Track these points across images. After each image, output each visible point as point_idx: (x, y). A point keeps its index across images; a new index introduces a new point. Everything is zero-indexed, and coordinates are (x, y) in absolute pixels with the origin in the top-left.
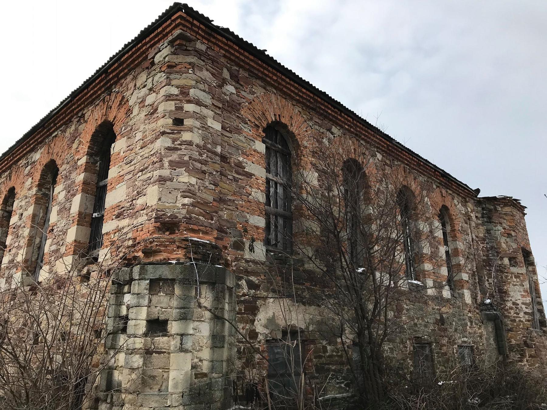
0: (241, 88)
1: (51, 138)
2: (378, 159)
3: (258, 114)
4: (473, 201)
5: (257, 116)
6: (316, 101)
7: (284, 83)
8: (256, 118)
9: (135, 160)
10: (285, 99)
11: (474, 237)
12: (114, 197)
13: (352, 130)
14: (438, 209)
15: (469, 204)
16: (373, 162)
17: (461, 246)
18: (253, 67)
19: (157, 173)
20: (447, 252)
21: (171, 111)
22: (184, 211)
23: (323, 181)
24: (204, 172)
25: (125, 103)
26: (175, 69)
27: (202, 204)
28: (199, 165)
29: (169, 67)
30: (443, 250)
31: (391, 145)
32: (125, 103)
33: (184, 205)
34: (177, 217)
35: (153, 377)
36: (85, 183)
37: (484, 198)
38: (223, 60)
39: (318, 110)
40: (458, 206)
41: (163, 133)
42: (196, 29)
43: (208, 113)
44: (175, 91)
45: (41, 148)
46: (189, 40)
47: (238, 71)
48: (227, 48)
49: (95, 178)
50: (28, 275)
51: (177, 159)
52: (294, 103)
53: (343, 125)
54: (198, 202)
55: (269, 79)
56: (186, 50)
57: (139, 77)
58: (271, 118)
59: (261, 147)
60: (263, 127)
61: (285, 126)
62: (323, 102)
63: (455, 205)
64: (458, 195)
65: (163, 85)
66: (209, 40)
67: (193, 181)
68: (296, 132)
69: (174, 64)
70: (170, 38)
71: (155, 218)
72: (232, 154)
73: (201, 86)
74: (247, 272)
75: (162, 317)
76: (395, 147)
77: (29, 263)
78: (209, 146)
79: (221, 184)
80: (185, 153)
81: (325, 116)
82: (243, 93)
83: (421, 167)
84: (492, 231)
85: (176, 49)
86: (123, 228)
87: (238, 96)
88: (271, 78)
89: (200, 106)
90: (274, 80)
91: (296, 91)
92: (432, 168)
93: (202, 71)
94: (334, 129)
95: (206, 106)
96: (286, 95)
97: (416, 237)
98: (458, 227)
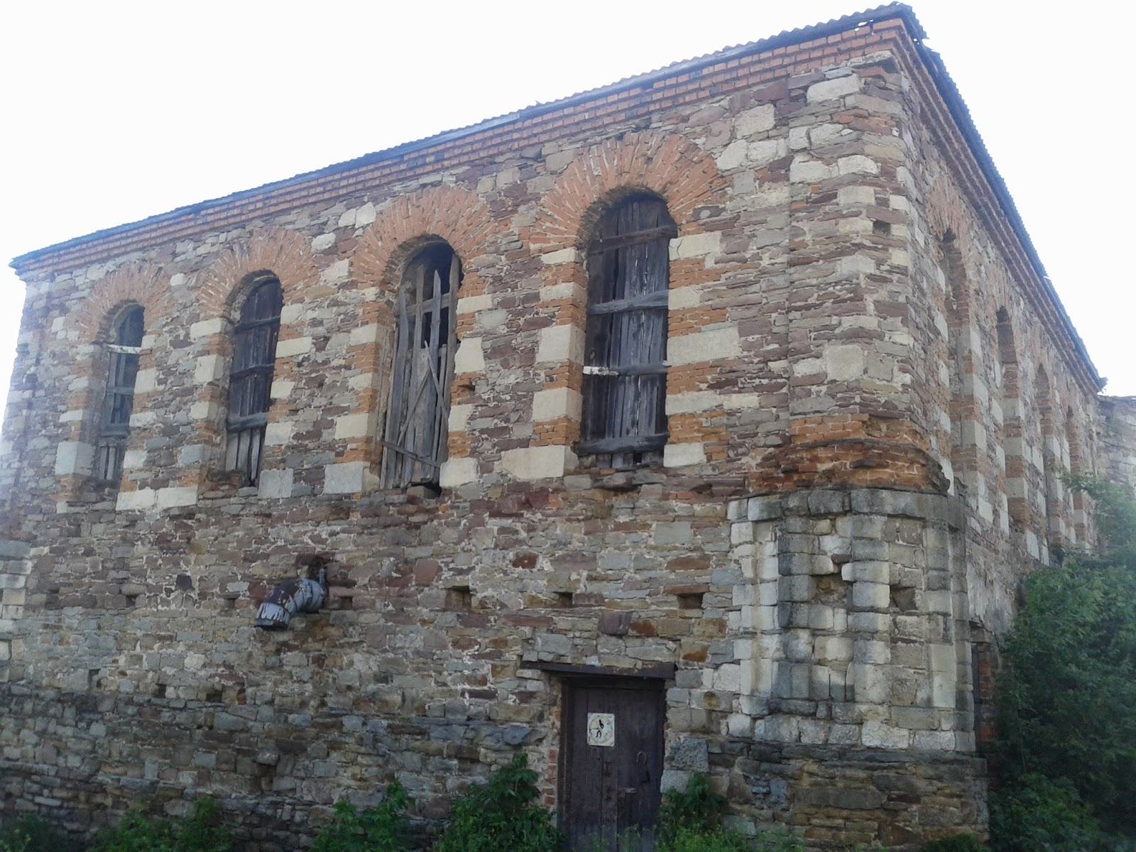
1: (414, 184)
21: (869, 206)
34: (896, 408)
51: (887, 299)
69: (866, 114)
70: (858, 60)
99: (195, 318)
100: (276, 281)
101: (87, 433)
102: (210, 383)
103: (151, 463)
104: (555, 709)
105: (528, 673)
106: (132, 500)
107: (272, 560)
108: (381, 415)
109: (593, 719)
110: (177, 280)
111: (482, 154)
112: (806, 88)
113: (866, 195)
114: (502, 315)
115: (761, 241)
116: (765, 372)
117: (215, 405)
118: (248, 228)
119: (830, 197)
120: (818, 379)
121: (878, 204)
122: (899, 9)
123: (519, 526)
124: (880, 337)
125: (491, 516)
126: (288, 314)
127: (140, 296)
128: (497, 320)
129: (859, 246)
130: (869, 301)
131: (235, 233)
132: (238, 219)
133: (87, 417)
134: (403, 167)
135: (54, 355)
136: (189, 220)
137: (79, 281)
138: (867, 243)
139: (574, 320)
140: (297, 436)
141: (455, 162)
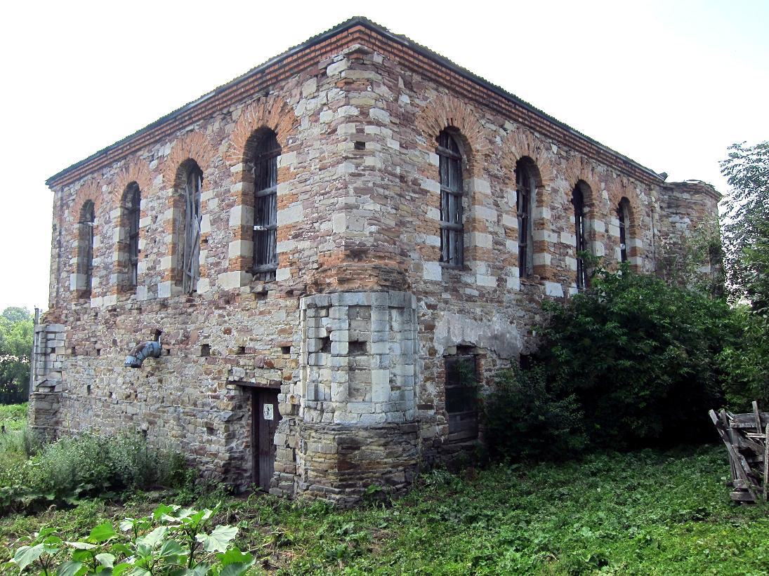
0: (415, 95)
1: (184, 131)
2: (553, 152)
3: (431, 122)
4: (658, 188)
5: (430, 125)
6: (489, 96)
7: (457, 82)
8: (429, 128)
9: (311, 180)
10: (458, 97)
11: (656, 232)
12: (285, 217)
13: (526, 122)
14: (617, 205)
15: (654, 193)
16: (546, 157)
17: (639, 243)
18: (426, 70)
19: (342, 201)
20: (623, 252)
21: (352, 134)
22: (372, 239)
23: (495, 187)
24: (386, 197)
25: (289, 112)
26: (353, 86)
27: (386, 230)
28: (381, 191)
29: (347, 83)
30: (618, 250)
31: (568, 134)
32: (289, 112)
33: (371, 233)
34: (365, 245)
35: (358, 390)
36: (244, 194)
38: (398, 69)
39: (491, 105)
40: (640, 197)
41: (346, 158)
42: (373, 41)
43: (387, 132)
44: (355, 112)
45: (170, 141)
46: (366, 53)
47: (412, 76)
48: (402, 54)
49: (252, 186)
50: (176, 284)
51: (362, 186)
52: (466, 101)
53: (517, 118)
54: (383, 229)
55: (442, 80)
56: (363, 64)
57: (305, 84)
59: (434, 159)
60: (436, 135)
61: (457, 130)
62: (497, 96)
63: (637, 196)
64: (642, 182)
65: (342, 104)
66: (384, 50)
67: (378, 207)
69: (351, 81)
70: (346, 51)
71: (345, 246)
72: (409, 172)
73: (380, 104)
74: (426, 293)
75: (361, 339)
76: (573, 136)
77: (176, 272)
78: (390, 169)
79: (401, 206)
80: (370, 180)
81: (498, 111)
82: (417, 101)
83: (601, 156)
84: (677, 224)
85: (352, 63)
86: (304, 250)
87: (412, 105)
88: (444, 79)
89: (380, 126)
90: (447, 81)
91: (469, 89)
92: (614, 155)
93: (380, 87)
94: (508, 125)
95: (385, 126)
96: (457, 94)
97: (576, 541)
98: (638, 222)
101: (81, 269)
102: (118, 242)
104: (249, 403)
105: (230, 387)
107: (143, 331)
108: (180, 256)
109: (266, 406)
111: (207, 113)
112: (326, 68)
115: (311, 156)
116: (312, 229)
117: (122, 253)
118: (128, 159)
119: (334, 131)
121: (357, 132)
122: (357, 20)
123: (225, 313)
124: (357, 207)
125: (216, 309)
127: (92, 198)
128: (213, 205)
131: (123, 162)
132: (122, 155)
133: (80, 261)
134: (177, 123)
135: (66, 230)
136: (104, 157)
138: (351, 156)
139: (244, 202)
141: (197, 118)
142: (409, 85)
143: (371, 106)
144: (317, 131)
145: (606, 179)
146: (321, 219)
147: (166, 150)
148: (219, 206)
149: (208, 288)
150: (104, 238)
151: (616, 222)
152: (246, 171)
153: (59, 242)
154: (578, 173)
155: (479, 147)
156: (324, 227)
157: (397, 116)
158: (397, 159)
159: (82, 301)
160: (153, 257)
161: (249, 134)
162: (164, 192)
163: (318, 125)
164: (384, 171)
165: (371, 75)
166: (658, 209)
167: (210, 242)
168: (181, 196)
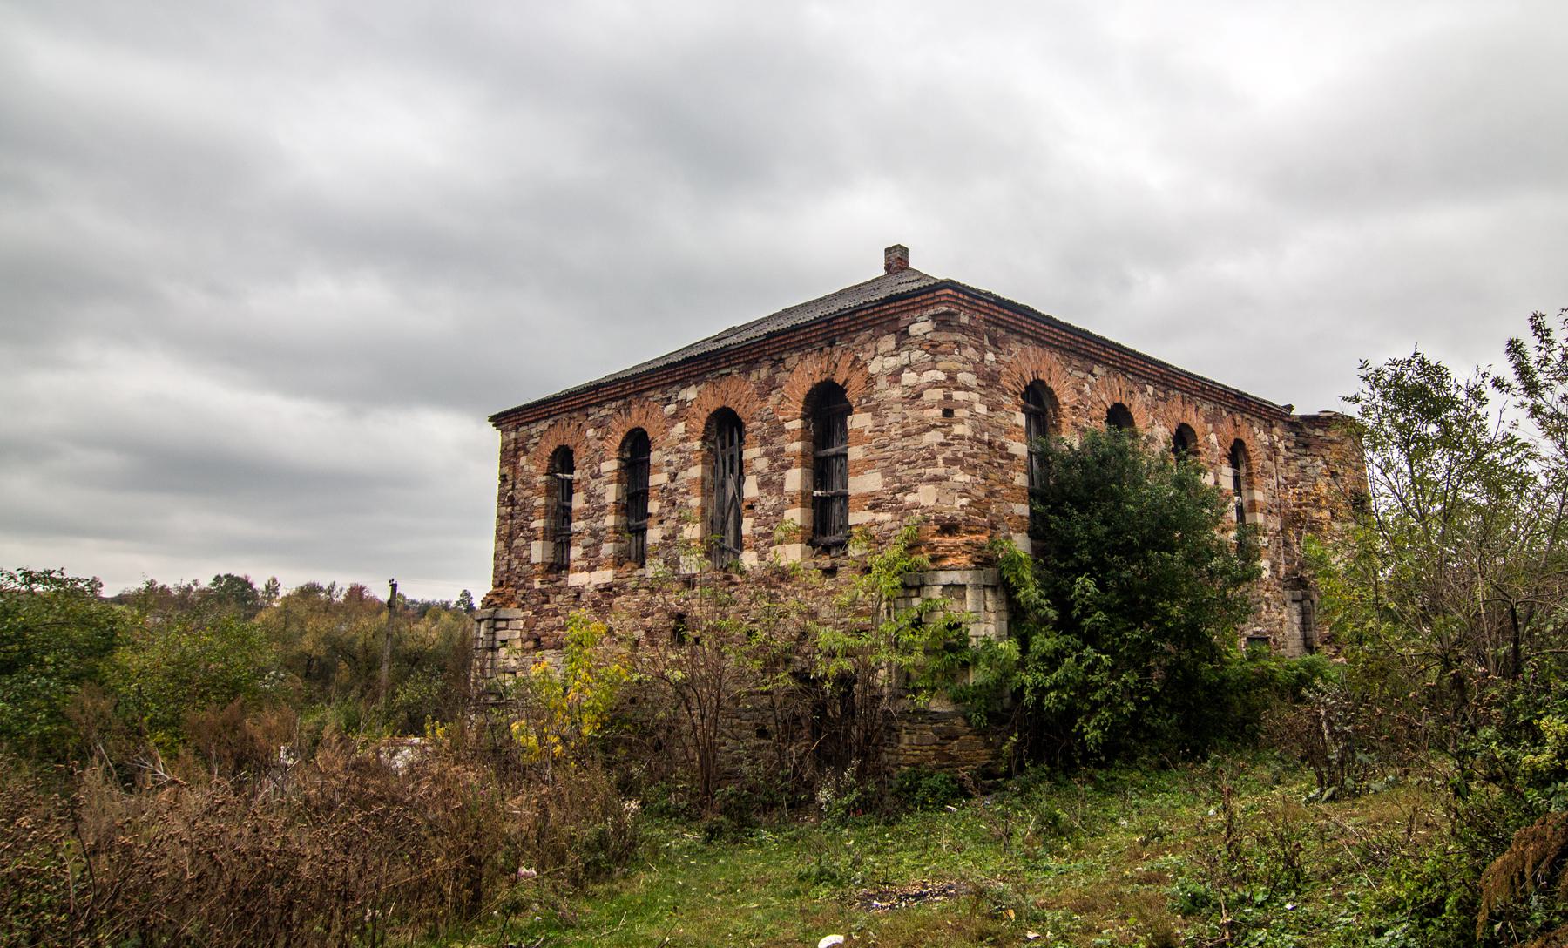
3: (1017, 377)
12: (865, 483)
15: (1277, 430)
17: (1259, 496)
24: (975, 467)
29: (933, 346)
36: (803, 455)
37: (1303, 418)
41: (934, 427)
43: (975, 396)
44: (941, 376)
46: (953, 314)
57: (882, 340)
58: (1029, 378)
59: (1021, 419)
61: (1043, 382)
67: (968, 478)
68: (1054, 387)
70: (931, 312)
80: (961, 449)
81: (1086, 356)
94: (1097, 370)
96: (1041, 342)
99: (602, 459)
100: (645, 433)
103: (585, 555)
106: (576, 579)
110: (590, 432)
113: (938, 394)
114: (765, 461)
116: (893, 500)
119: (919, 396)
120: (916, 506)
126: (655, 457)
127: (570, 443)
128: (762, 464)
129: (934, 427)
130: (940, 459)
131: (620, 402)
135: (523, 482)
137: (533, 431)
139: (803, 465)
140: (664, 538)
142: (993, 342)
143: (959, 371)
144: (896, 393)
145: (1213, 419)
146: (905, 490)
147: (690, 394)
148: (770, 467)
149: (755, 563)
150: (591, 496)
151: (1227, 471)
152: (805, 428)
153: (512, 498)
154: (1179, 415)
155: (1065, 399)
156: (910, 499)
157: (984, 378)
158: (985, 425)
159: (553, 577)
160: (669, 524)
161: (808, 388)
162: (688, 445)
163: (895, 379)
164: (973, 439)
165: (959, 337)
166: (1283, 450)
167: (758, 508)
168: (710, 450)
